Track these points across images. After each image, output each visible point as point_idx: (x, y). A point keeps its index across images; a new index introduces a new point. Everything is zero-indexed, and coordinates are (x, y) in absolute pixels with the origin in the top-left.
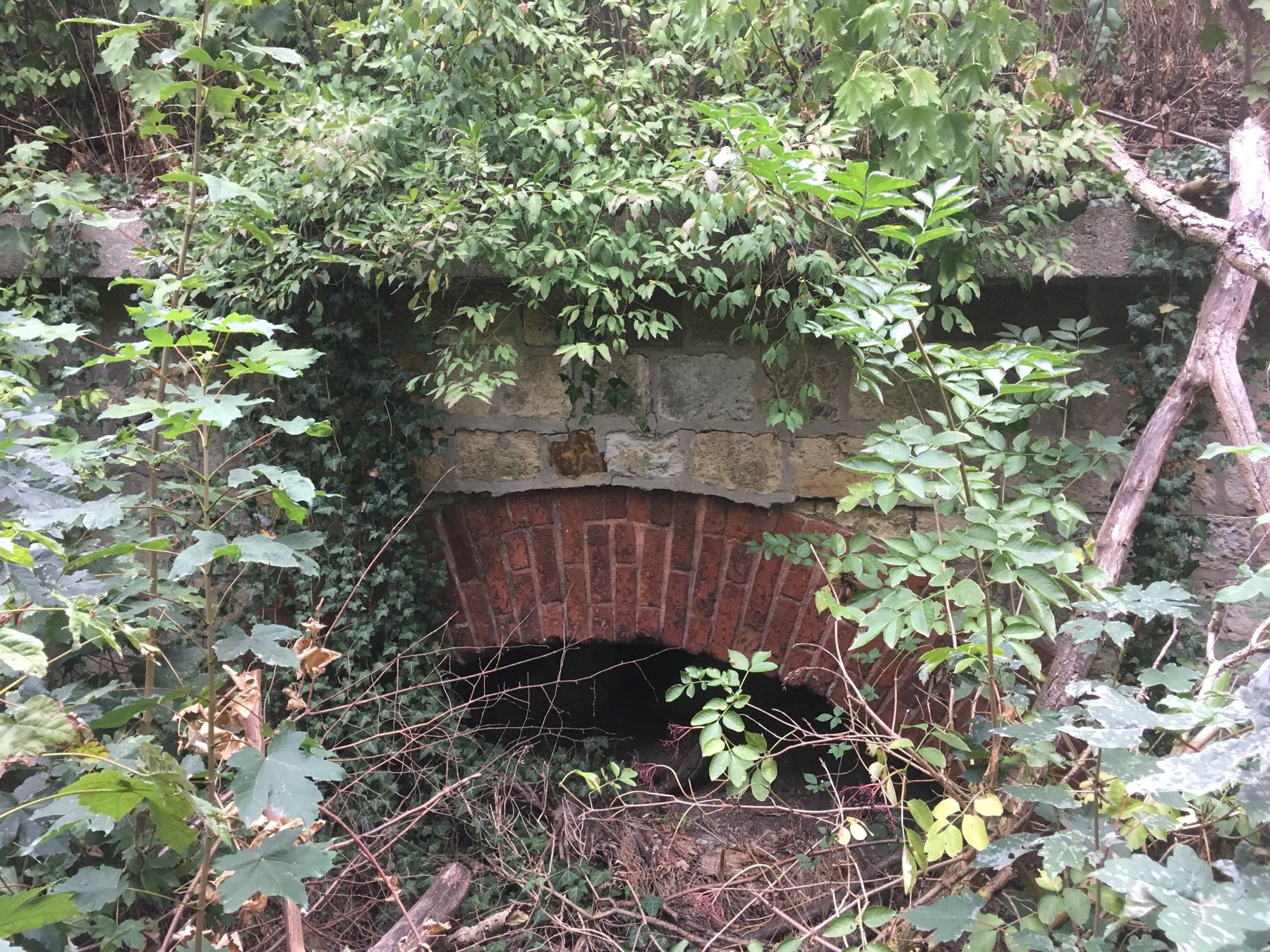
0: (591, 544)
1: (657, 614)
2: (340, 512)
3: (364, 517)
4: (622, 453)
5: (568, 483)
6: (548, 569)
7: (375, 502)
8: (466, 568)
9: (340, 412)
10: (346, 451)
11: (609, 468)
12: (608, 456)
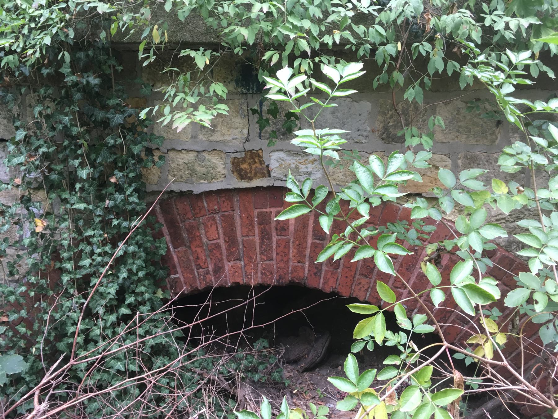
0: (260, 224)
1: (303, 268)
2: (91, 207)
3: (108, 210)
4: (281, 165)
5: (245, 185)
6: (231, 240)
7: (114, 200)
8: (177, 240)
9: (87, 137)
10: (93, 165)
11: (272, 174)
12: (271, 167)
